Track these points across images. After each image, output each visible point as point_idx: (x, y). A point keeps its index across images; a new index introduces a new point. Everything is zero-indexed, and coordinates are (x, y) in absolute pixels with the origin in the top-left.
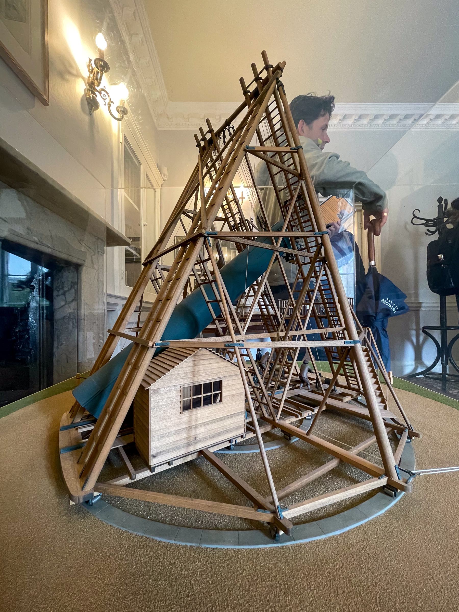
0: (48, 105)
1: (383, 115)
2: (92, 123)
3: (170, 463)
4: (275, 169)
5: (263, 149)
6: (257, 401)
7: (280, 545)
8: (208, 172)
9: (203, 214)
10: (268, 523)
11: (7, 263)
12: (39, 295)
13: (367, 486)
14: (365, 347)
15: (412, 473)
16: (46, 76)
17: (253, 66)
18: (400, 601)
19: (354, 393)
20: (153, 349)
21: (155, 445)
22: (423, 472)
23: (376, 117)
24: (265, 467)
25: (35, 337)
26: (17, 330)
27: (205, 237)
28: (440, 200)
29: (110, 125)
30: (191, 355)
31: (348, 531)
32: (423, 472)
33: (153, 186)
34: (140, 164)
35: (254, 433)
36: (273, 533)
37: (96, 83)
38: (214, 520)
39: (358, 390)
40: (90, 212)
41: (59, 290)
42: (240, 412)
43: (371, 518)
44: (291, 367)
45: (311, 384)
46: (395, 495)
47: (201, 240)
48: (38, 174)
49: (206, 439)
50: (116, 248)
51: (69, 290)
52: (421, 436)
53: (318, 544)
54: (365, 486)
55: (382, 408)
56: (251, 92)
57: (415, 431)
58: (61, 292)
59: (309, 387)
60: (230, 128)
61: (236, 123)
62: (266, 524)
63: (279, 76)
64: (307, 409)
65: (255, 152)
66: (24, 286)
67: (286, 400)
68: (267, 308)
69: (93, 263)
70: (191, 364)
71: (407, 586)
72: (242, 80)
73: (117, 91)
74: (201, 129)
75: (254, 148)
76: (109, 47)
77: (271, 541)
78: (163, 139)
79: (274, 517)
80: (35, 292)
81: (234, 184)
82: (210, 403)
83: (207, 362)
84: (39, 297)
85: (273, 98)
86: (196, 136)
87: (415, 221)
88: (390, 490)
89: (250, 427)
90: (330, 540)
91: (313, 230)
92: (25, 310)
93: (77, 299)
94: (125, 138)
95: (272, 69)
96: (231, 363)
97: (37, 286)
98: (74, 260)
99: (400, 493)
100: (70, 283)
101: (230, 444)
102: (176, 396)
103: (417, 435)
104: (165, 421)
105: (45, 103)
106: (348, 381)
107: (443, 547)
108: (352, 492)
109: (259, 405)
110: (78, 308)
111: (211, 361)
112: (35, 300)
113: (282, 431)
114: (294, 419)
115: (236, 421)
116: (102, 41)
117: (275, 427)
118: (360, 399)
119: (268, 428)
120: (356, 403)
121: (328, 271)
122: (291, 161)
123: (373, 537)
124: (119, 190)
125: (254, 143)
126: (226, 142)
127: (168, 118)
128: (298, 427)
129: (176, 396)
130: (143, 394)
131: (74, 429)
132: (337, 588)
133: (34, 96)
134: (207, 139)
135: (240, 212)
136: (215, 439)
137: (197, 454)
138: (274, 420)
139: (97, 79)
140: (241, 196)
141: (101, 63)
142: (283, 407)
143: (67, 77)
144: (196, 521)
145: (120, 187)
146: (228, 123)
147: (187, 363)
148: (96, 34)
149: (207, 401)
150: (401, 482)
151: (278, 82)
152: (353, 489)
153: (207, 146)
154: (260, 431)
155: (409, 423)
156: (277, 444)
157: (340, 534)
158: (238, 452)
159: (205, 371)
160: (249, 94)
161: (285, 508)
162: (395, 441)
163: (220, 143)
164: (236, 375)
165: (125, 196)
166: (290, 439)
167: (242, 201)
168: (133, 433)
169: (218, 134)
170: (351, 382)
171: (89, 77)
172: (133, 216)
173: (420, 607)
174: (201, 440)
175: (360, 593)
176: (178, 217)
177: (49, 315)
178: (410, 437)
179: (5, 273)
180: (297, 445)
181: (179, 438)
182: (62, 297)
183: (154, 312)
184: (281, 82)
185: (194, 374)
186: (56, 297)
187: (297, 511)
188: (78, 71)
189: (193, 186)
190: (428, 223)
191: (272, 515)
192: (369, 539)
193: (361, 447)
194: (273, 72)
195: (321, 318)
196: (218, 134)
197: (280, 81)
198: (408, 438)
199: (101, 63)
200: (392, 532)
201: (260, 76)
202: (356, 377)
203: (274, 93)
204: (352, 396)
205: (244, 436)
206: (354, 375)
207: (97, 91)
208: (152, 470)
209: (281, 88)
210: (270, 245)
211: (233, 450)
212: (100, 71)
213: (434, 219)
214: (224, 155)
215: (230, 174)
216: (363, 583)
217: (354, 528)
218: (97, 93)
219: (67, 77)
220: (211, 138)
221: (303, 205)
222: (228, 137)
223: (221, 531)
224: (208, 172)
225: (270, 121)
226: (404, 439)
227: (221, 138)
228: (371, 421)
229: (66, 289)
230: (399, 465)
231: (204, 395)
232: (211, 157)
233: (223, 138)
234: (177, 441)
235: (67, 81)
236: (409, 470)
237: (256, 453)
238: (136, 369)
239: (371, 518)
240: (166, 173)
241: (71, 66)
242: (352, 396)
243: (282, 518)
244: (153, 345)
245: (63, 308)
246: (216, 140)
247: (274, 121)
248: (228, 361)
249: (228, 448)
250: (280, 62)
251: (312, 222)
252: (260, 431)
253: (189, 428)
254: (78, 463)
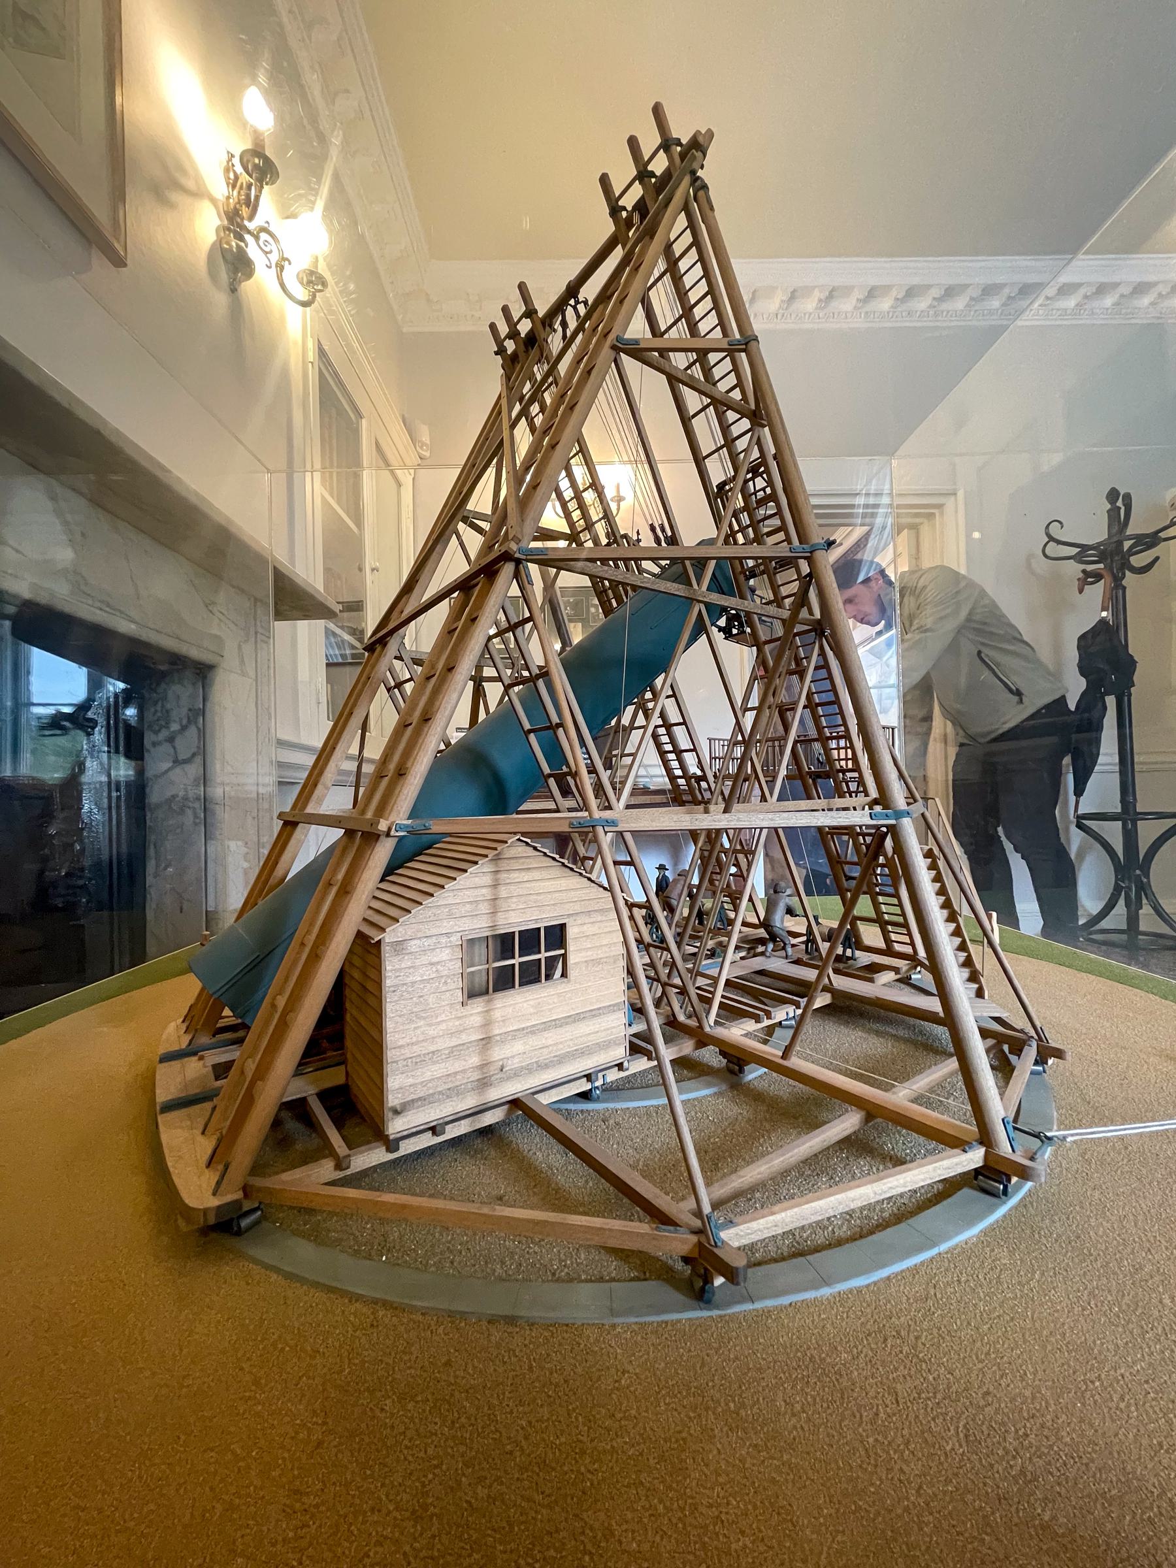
0: (125, 265)
1: (966, 286)
2: (237, 309)
3: (438, 1128)
4: (693, 401)
5: (658, 343)
6: (658, 980)
7: (715, 1313)
8: (524, 412)
9: (512, 508)
10: (686, 1260)
11: (29, 673)
12: (109, 746)
13: (934, 1170)
14: (926, 848)
15: (1046, 1137)
16: (118, 195)
17: (633, 143)
18: (1017, 1431)
19: (903, 964)
20: (390, 839)
21: (398, 1084)
22: (1072, 1135)
23: (950, 292)
24: (683, 1149)
25: (99, 849)
26: (52, 831)
27: (518, 562)
28: (1113, 495)
29: (282, 319)
30: (486, 856)
31: (888, 1278)
32: (1072, 1135)
33: (388, 464)
34: (360, 416)
35: (650, 1059)
36: (699, 1283)
37: (245, 212)
38: (551, 1260)
39: (913, 958)
40: (233, 530)
41: (159, 730)
42: (614, 1005)
43: (944, 1247)
44: (740, 899)
45: (793, 946)
46: (1005, 1192)
47: (508, 569)
48: (98, 432)
49: (529, 1070)
50: (303, 625)
51: (184, 728)
52: (1069, 1056)
53: (812, 1310)
54: (930, 1167)
55: (973, 994)
56: (629, 209)
57: (1053, 1044)
58: (164, 734)
59: (789, 950)
60: (577, 302)
61: (590, 291)
62: (679, 1265)
63: (695, 165)
64: (785, 1001)
65: (637, 352)
66: (67, 724)
67: (728, 983)
68: (680, 760)
69: (242, 662)
70: (487, 880)
71: (1034, 1398)
72: (604, 181)
73: (299, 234)
74: (506, 310)
75: (636, 342)
76: (280, 119)
77: (694, 1303)
78: (416, 356)
79: (700, 1243)
80: (99, 736)
81: (589, 432)
82: (537, 980)
83: (525, 876)
84: (109, 752)
85: (682, 221)
86: (493, 327)
87: (1052, 549)
88: (992, 1178)
89: (639, 1046)
90: (841, 1297)
91: (788, 540)
92: (72, 785)
93: (202, 752)
94: (322, 352)
95: (679, 149)
96: (589, 879)
97: (101, 721)
98: (195, 653)
99: (1018, 1187)
100: (184, 711)
101: (588, 1086)
102: (451, 960)
103: (1059, 1054)
104: (422, 1023)
105: (119, 262)
106: (886, 934)
107: (1124, 1307)
108: (895, 1183)
109: (664, 993)
110: (205, 779)
111: (536, 875)
112: (103, 769)
113: (723, 1053)
114: (750, 1026)
115: (604, 1025)
116: (259, 110)
117: (705, 1045)
118: (918, 979)
119: (686, 1047)
120: (907, 989)
121: (830, 654)
122: (732, 380)
123: (949, 1290)
124: (308, 475)
125: (637, 329)
126: (569, 334)
127: (428, 300)
128: (765, 1042)
129: (451, 960)
130: (367, 951)
131: (196, 1058)
132: (859, 1407)
133: (89, 242)
134: (523, 335)
135: (607, 516)
136: (550, 1071)
137: (506, 1107)
138: (701, 1027)
139: (248, 203)
140: (614, 494)
141: (257, 161)
142: (723, 997)
143: (175, 197)
144: (503, 1263)
145: (308, 467)
146: (572, 290)
147: (477, 878)
148: (243, 88)
149: (531, 976)
150: (1019, 1158)
151: (695, 179)
152: (898, 1177)
153: (522, 351)
154: (667, 1054)
155: (1038, 1024)
156: (709, 1085)
157: (868, 1286)
158: (611, 1105)
159: (523, 899)
160: (624, 214)
161: (730, 1223)
162: (1004, 1069)
163: (555, 342)
164: (601, 911)
165: (323, 497)
166: (741, 1071)
167: (619, 506)
168: (343, 1062)
169: (547, 322)
170: (893, 937)
171: (228, 198)
172: (344, 547)
173: (1066, 1444)
174: (516, 1074)
175: (917, 1417)
176: (451, 528)
177: (136, 796)
178: (1041, 1060)
179: (24, 700)
180: (762, 1086)
181: (458, 1066)
182: (166, 748)
183: (392, 754)
184: (702, 180)
185: (495, 906)
186: (152, 750)
187: (759, 1230)
188: (198, 179)
189: (490, 448)
190: (1083, 552)
191: (694, 1239)
192: (939, 1296)
193: (922, 1083)
194: (683, 156)
195: (816, 776)
196: (547, 322)
197: (699, 178)
198: (1036, 1063)
199: (257, 161)
200: (999, 1277)
201: (649, 168)
202: (906, 925)
203: (686, 208)
204: (896, 970)
205: (626, 1064)
206: (901, 920)
207: (249, 232)
208: (391, 1145)
209: (701, 193)
210: (681, 586)
211: (598, 1100)
212: (257, 180)
213: (1100, 544)
214: (563, 367)
215: (578, 408)
216: (923, 1395)
217: (902, 1271)
218: (247, 237)
219: (175, 197)
220: (531, 330)
221: (764, 489)
222: (572, 324)
223: (565, 1285)
224: (524, 412)
225: (677, 280)
226: (1026, 1064)
227: (555, 331)
228: (945, 1025)
229: (175, 727)
230: (1016, 1120)
231: (524, 957)
232: (531, 378)
233: (560, 329)
234: (456, 1073)
235: (171, 206)
236: (1037, 1130)
237: (657, 1107)
238: (347, 893)
239: (944, 1247)
240: (426, 439)
241: (184, 171)
242: (896, 970)
243: (719, 1244)
244: (390, 829)
245: (171, 780)
246: (543, 335)
247: (688, 281)
248: (581, 874)
249: (585, 1096)
250: (698, 132)
251: (787, 534)
252: (667, 1054)
253: (486, 1042)
254: (203, 1133)
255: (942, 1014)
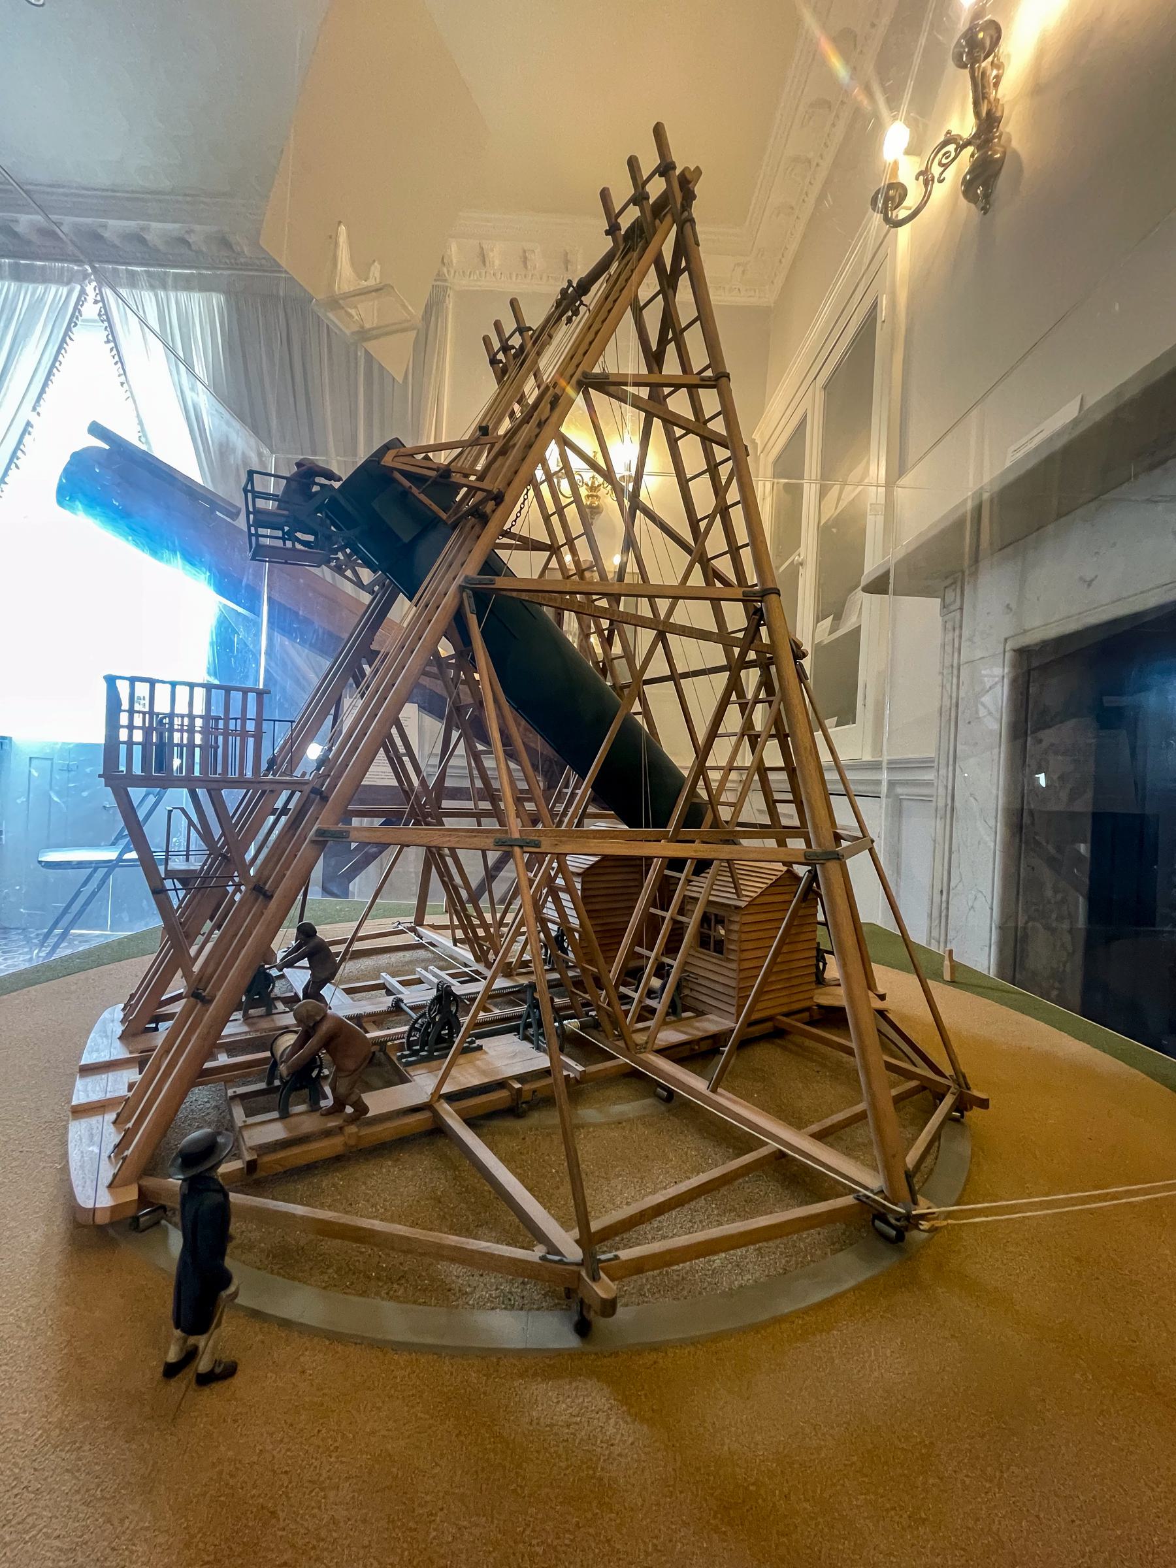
74: (498, 326)
86: (486, 340)
255: (180, 973)
